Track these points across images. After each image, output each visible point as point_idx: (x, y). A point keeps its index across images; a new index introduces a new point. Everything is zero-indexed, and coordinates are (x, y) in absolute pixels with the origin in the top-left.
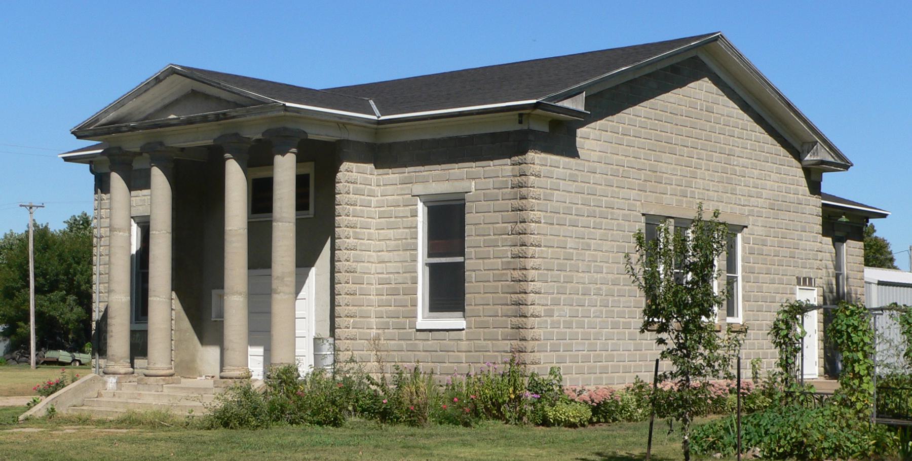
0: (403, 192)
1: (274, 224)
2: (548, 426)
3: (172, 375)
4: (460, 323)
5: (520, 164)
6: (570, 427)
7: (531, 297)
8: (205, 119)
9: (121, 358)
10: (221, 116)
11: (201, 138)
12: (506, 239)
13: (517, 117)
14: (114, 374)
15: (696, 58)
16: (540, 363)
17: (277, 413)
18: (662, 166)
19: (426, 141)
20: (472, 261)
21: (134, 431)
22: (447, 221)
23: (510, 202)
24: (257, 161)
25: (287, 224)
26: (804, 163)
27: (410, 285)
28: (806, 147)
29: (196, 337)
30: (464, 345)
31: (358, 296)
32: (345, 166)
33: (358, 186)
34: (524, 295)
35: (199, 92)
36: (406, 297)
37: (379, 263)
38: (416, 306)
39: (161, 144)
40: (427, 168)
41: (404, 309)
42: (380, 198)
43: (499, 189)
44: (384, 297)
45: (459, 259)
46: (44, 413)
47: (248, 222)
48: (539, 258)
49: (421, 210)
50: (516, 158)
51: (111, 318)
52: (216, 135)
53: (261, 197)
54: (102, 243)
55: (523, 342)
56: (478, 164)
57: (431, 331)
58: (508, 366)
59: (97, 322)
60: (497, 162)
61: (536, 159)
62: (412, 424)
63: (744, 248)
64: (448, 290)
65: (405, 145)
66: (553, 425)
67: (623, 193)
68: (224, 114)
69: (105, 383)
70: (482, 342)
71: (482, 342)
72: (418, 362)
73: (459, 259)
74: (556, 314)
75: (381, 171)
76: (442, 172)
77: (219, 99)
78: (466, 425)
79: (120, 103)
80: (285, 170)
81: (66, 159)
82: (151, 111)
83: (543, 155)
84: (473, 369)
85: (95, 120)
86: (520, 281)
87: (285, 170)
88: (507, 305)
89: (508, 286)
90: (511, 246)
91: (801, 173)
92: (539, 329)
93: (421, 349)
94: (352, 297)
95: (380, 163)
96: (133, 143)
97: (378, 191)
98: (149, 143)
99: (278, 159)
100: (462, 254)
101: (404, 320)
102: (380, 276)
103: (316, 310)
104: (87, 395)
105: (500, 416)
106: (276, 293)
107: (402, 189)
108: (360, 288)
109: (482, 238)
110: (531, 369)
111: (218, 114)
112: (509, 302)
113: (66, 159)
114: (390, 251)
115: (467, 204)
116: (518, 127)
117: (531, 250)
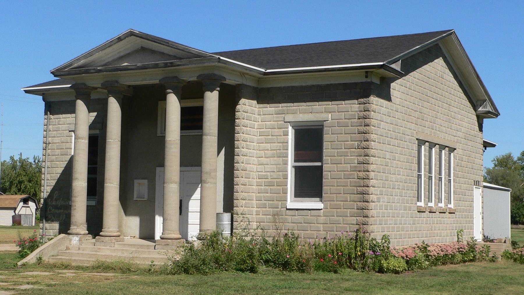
1: (204, 137)
2: (383, 273)
3: (119, 236)
4: (318, 205)
5: (365, 103)
6: (396, 273)
7: (371, 190)
8: (156, 66)
9: (81, 224)
10: (169, 64)
11: (150, 78)
12: (354, 152)
13: (364, 73)
14: (77, 234)
15: (437, 45)
16: (376, 232)
17: (219, 264)
18: (425, 110)
20: (328, 165)
21: (155, 278)
22: (310, 140)
23: (357, 128)
24: (192, 95)
25: (213, 137)
26: (478, 112)
27: (282, 180)
28: (479, 103)
29: (122, 211)
30: (322, 219)
31: (247, 186)
32: (243, 101)
33: (249, 114)
34: (367, 188)
35: (147, 49)
36: (279, 187)
37: (259, 165)
38: (287, 193)
39: (117, 82)
40: (295, 104)
41: (277, 195)
42: (260, 123)
43: (349, 119)
44: (263, 187)
45: (319, 164)
46: (34, 261)
48: (375, 164)
49: (291, 132)
50: (362, 100)
51: (75, 197)
52: (160, 77)
53: (192, 119)
54: (50, 147)
55: (366, 219)
56: (333, 102)
57: (297, 210)
59: (45, 200)
60: (347, 102)
61: (373, 99)
62: (303, 271)
63: (454, 162)
64: (310, 183)
65: (280, 89)
66: (386, 272)
67: (409, 125)
68: (171, 63)
69: (71, 240)
70: (335, 218)
71: (335, 218)
72: (289, 230)
73: (319, 164)
74: (381, 200)
75: (261, 105)
76: (307, 107)
77: (162, 54)
78: (336, 272)
79: (90, 54)
80: (212, 101)
81: (26, 92)
82: (110, 60)
83: (377, 99)
84: (328, 235)
85: (71, 64)
86: (364, 179)
87: (212, 101)
88: (354, 194)
89: (355, 182)
90: (357, 156)
91: (475, 118)
92: (375, 210)
93: (290, 221)
94: (245, 186)
95: (260, 101)
96: (95, 81)
97: (259, 118)
99: (208, 94)
100: (320, 159)
102: (260, 173)
103: (511, 199)
104: (60, 248)
105: (352, 267)
106: (205, 183)
107: (277, 117)
108: (249, 181)
109: (336, 150)
110: (372, 236)
111: (167, 63)
112: (355, 192)
113: (26, 92)
115: (325, 128)
116: (364, 80)
117: (372, 159)
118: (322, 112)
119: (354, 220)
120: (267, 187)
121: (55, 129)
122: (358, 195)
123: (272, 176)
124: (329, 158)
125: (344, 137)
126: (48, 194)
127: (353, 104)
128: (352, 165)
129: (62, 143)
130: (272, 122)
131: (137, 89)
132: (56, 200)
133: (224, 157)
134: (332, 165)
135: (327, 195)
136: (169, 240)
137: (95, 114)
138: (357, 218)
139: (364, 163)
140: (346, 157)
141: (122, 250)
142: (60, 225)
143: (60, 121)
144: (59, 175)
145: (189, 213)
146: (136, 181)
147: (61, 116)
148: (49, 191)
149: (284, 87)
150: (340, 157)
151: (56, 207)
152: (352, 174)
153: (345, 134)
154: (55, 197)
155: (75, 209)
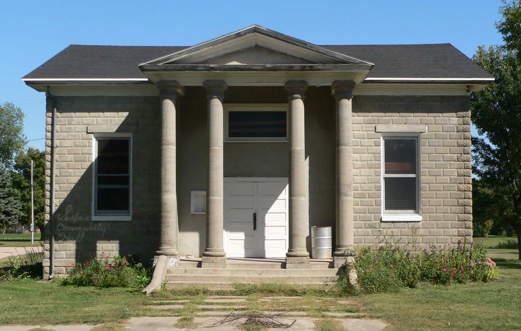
0: (368, 129)
4: (417, 217)
5: (464, 117)
10: (307, 68)
12: (454, 164)
19: (386, 96)
27: (375, 191)
40: (387, 114)
41: (369, 207)
43: (447, 132)
45: (413, 176)
47: (224, 143)
49: (94, 144)
50: (461, 113)
51: (168, 212)
56: (430, 114)
57: (393, 222)
58: (457, 245)
60: (444, 114)
68: (311, 67)
73: (413, 176)
76: (401, 118)
82: (212, 56)
88: (455, 206)
89: (456, 194)
90: (457, 168)
98: (208, 81)
101: (370, 215)
114: (357, 168)
118: (418, 124)
119: (455, 231)
120: (357, 199)
121: (64, 130)
122: (459, 207)
123: (363, 187)
124: (427, 170)
125: (441, 149)
126: (57, 208)
127: (451, 117)
128: (451, 177)
129: (76, 146)
130: (361, 132)
131: (188, 89)
132: (70, 215)
133: (308, 167)
134: (430, 177)
135: (426, 207)
136: (304, 258)
137: (126, 114)
138: (459, 229)
139: (465, 176)
140: (445, 170)
141: (248, 270)
142: (77, 244)
143: (72, 120)
144: (72, 186)
145: (266, 228)
146: (193, 193)
147: (73, 114)
148: (58, 205)
149: (374, 96)
150: (438, 169)
151: (70, 224)
152: (452, 186)
153: (443, 146)
154: (67, 212)
155: (168, 226)
